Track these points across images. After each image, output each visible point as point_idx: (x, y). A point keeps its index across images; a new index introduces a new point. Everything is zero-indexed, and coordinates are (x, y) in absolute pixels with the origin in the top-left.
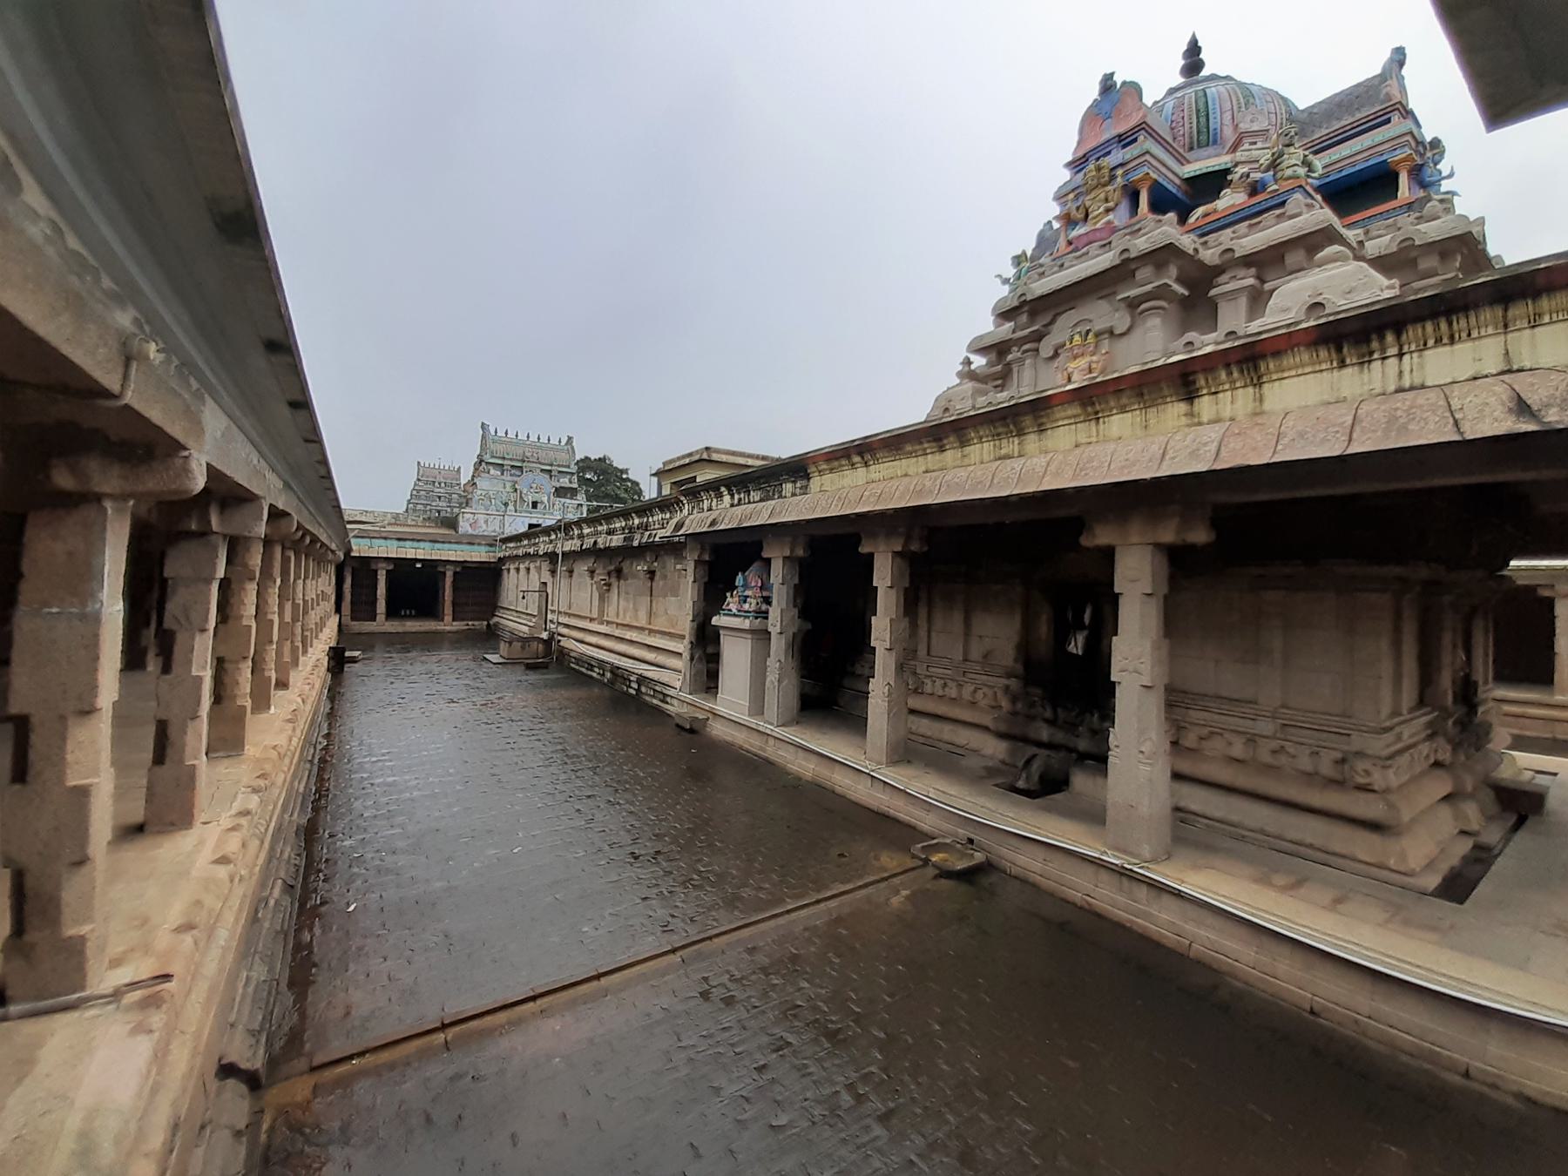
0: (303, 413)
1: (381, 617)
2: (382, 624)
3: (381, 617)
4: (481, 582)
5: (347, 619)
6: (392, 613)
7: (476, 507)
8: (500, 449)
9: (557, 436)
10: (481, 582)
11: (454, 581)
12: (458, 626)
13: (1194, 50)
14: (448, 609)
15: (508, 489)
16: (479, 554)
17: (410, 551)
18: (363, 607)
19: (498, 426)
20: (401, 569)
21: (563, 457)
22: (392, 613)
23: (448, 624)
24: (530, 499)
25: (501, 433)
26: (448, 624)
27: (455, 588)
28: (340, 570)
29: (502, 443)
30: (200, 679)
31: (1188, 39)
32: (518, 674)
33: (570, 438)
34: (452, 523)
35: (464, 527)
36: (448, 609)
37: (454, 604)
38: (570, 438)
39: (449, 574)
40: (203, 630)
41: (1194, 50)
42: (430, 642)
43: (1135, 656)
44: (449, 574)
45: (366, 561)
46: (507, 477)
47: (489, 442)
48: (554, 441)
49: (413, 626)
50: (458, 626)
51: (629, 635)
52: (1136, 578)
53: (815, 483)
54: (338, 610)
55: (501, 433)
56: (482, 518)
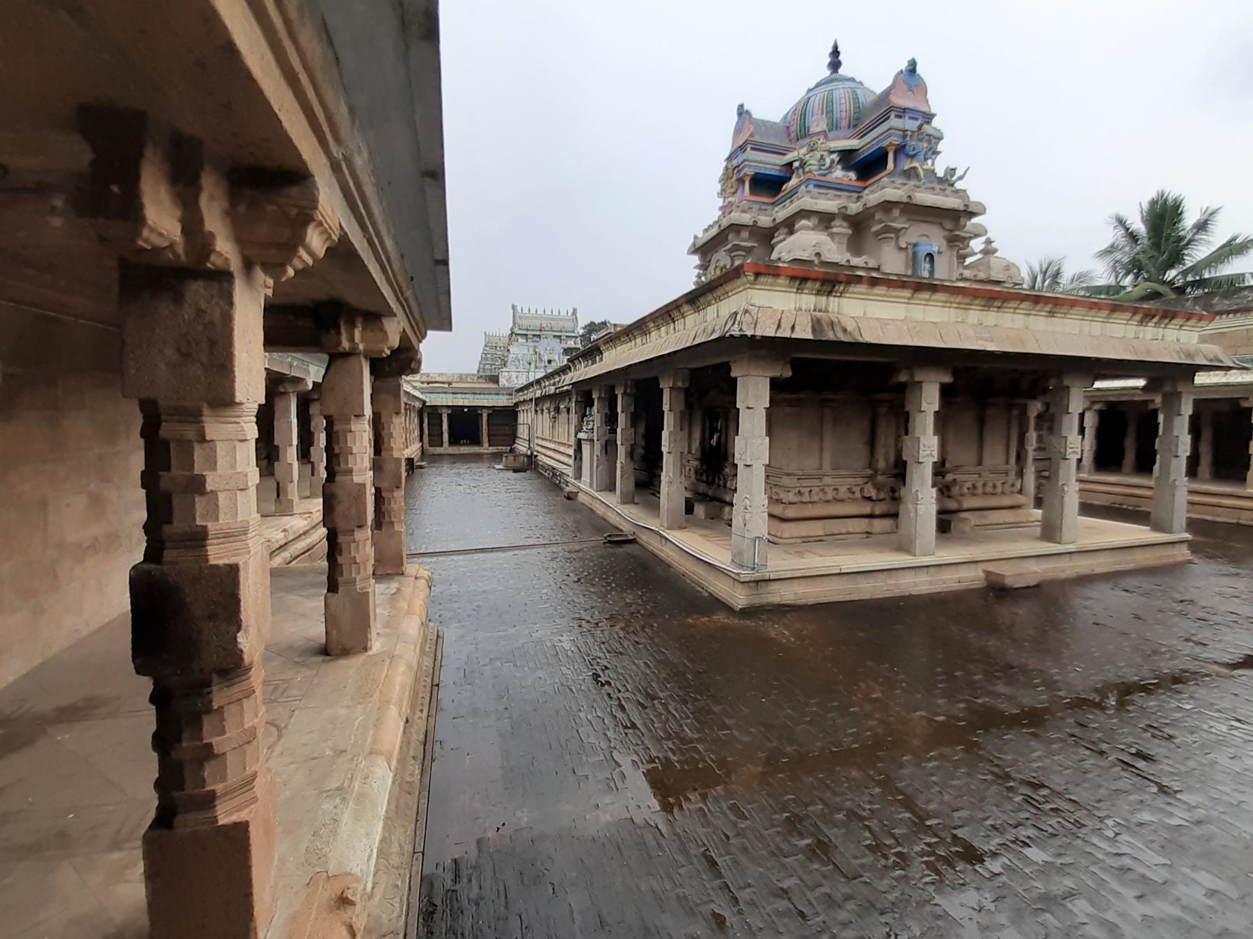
0: (441, 268)
1: (446, 444)
2: (446, 448)
3: (446, 444)
4: (506, 419)
5: (426, 446)
6: (454, 441)
7: (510, 367)
8: (525, 323)
9: (566, 310)
10: (506, 419)
11: (488, 420)
12: (492, 449)
13: (835, 52)
14: (485, 438)
15: (531, 352)
16: (502, 401)
17: (460, 401)
18: (436, 439)
19: (524, 306)
20: (457, 413)
21: (569, 325)
22: (451, 444)
23: (486, 448)
24: (546, 358)
25: (526, 311)
26: (486, 448)
27: (489, 425)
28: (420, 413)
29: (527, 318)
30: (362, 486)
31: (832, 44)
32: (511, 475)
33: (575, 310)
34: (495, 379)
35: (503, 382)
36: (485, 438)
37: (489, 435)
38: (575, 310)
39: (485, 415)
40: (360, 416)
41: (835, 52)
42: (478, 457)
43: (752, 444)
44: (485, 415)
45: (435, 408)
46: (530, 344)
47: (518, 319)
48: (563, 313)
49: (464, 450)
50: (492, 449)
51: (562, 449)
52: (753, 395)
53: (605, 355)
54: (421, 440)
55: (526, 311)
56: (514, 375)
